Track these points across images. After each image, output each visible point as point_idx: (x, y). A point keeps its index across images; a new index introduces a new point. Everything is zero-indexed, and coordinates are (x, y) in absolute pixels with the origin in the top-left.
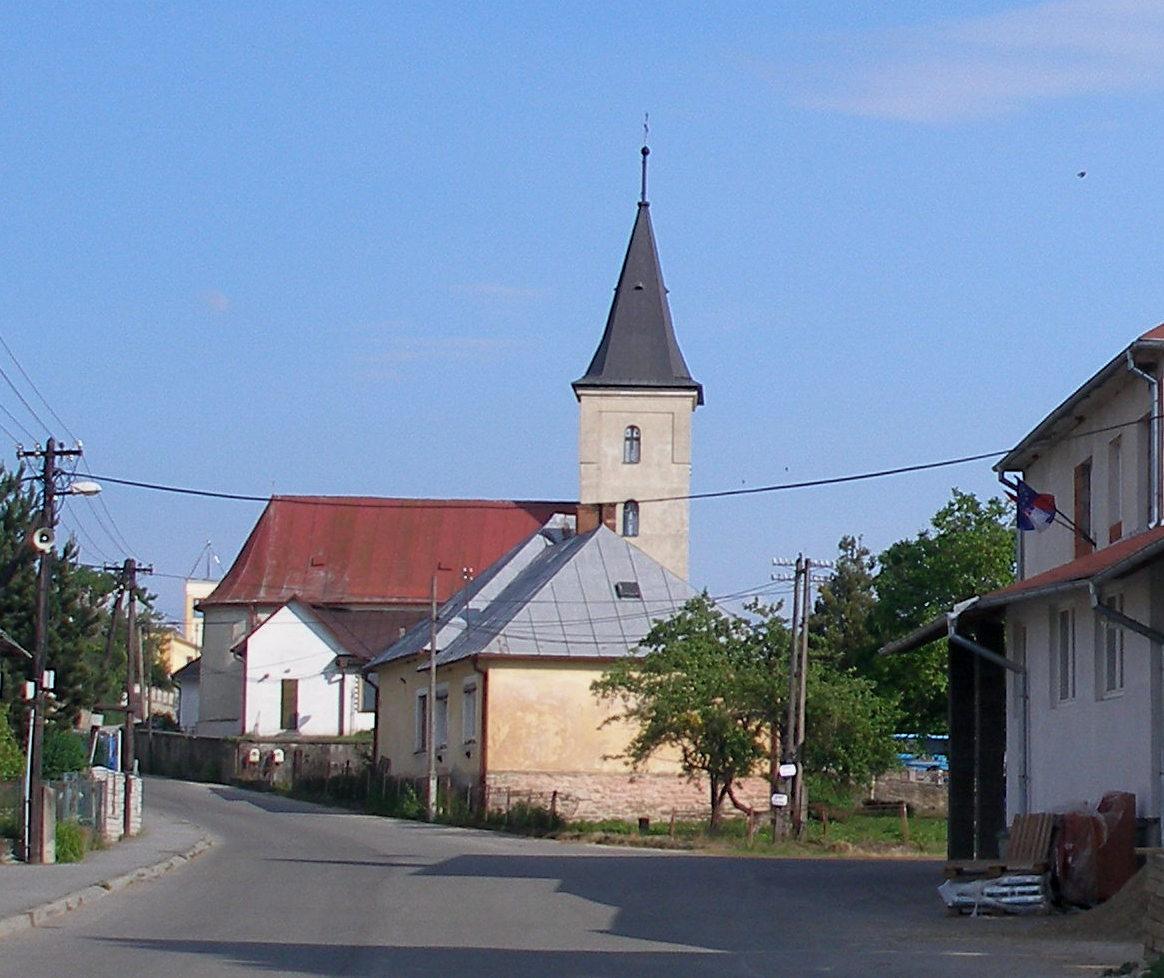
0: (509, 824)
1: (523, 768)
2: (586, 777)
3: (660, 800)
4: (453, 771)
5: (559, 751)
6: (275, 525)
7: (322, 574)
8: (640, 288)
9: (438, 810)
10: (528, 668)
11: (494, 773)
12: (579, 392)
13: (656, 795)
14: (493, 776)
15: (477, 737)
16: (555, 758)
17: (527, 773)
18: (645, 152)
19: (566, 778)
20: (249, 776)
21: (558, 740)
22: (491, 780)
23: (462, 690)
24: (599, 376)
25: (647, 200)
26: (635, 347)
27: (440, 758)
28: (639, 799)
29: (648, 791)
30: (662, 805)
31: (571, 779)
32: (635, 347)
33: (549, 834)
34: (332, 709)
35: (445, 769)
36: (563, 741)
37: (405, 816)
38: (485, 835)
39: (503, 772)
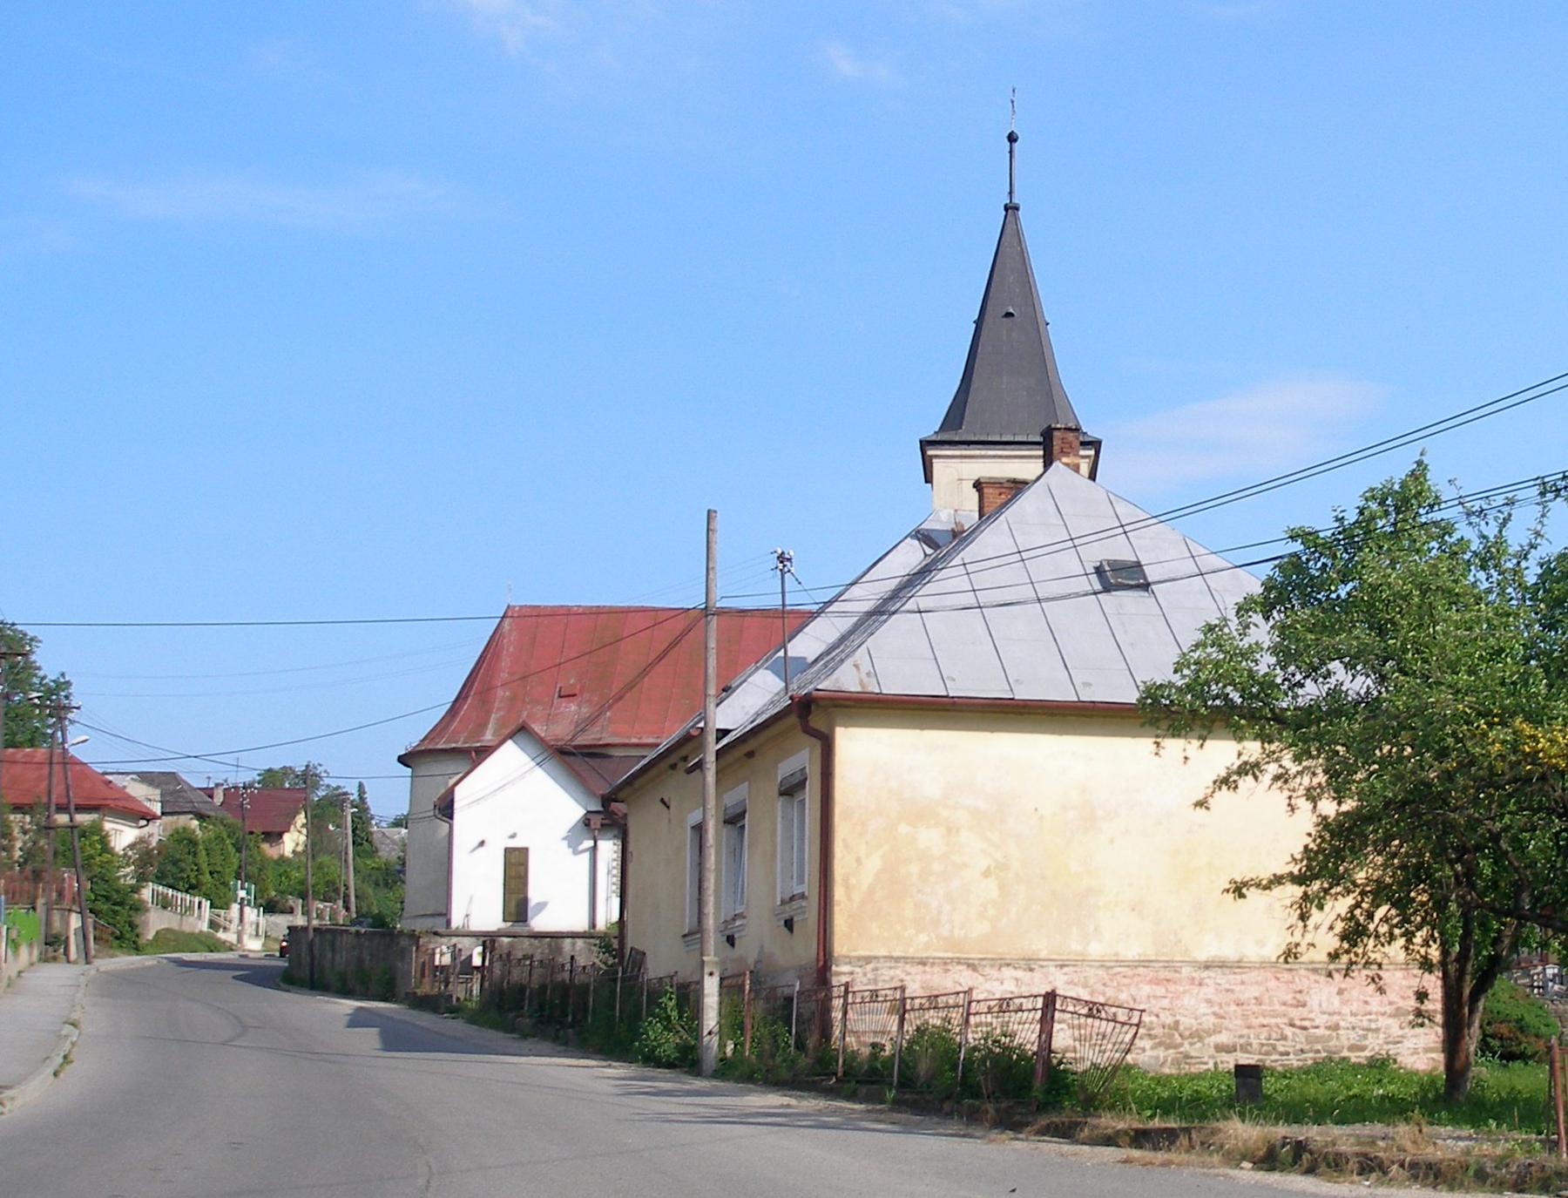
0: (907, 1083)
1: (911, 952)
2: (1052, 969)
3: (1212, 1019)
4: (757, 962)
5: (991, 912)
6: (509, 646)
7: (573, 707)
8: (1011, 315)
9: (722, 1046)
10: (922, 728)
11: (850, 960)
12: (930, 453)
13: (1204, 1009)
14: (845, 968)
15: (810, 887)
16: (983, 928)
17: (923, 962)
18: (1012, 138)
19: (1008, 973)
20: (426, 988)
21: (991, 888)
22: (841, 973)
23: (774, 789)
24: (957, 430)
25: (1015, 200)
26: (1009, 398)
27: (731, 940)
28: (1169, 1020)
29: (1187, 1001)
30: (1216, 1030)
31: (1020, 974)
32: (1009, 398)
33: (1043, 1121)
34: (573, 894)
35: (741, 960)
36: (1001, 887)
37: (652, 1060)
38: (849, 1124)
39: (868, 960)
